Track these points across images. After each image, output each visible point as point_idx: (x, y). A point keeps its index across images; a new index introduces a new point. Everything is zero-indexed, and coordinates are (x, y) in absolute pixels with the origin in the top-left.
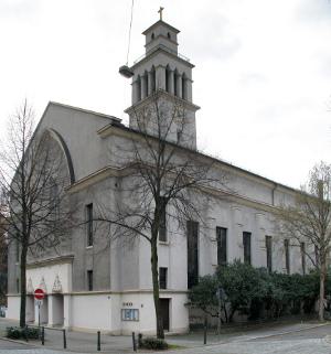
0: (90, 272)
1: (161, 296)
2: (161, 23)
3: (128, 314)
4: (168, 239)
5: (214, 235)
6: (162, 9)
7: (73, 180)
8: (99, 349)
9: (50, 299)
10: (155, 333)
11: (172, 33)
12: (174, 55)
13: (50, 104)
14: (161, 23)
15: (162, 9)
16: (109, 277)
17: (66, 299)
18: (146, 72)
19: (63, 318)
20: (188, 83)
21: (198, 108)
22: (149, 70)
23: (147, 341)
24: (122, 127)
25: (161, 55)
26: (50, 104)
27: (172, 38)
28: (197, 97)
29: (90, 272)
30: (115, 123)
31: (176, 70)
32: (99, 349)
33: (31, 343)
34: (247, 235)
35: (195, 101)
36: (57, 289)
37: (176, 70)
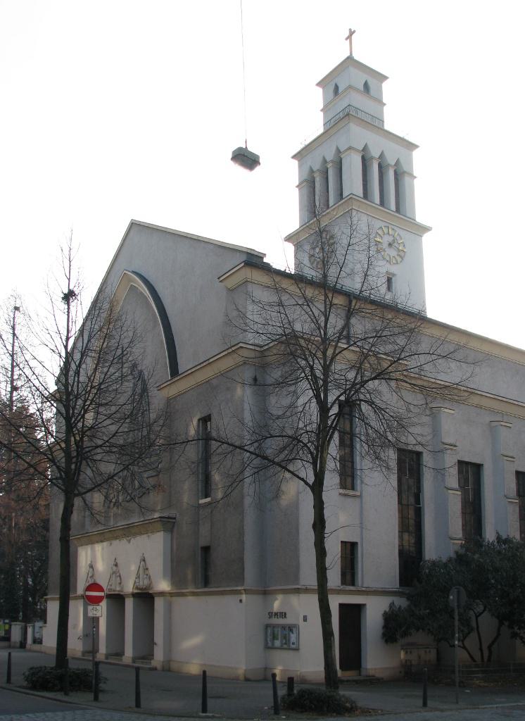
0: (206, 550)
1: (90, 614)
2: (350, 61)
3: (293, 644)
4: (359, 488)
5: (453, 480)
6: (352, 33)
7: (174, 371)
8: (204, 709)
9: (129, 604)
10: (323, 675)
11: (372, 83)
12: (375, 124)
13: (134, 226)
14: (350, 61)
15: (352, 33)
16: (242, 560)
17: (159, 604)
18: (325, 161)
19: (152, 643)
20: (407, 179)
21: (426, 229)
22: (330, 156)
23: (303, 693)
24: (267, 269)
25: (354, 128)
26: (134, 226)
27: (372, 92)
28: (423, 208)
29: (206, 550)
30: (254, 261)
31: (382, 156)
32: (204, 709)
33: (76, 697)
34: (471, 473)
35: (421, 217)
36: (144, 583)
37: (382, 156)
